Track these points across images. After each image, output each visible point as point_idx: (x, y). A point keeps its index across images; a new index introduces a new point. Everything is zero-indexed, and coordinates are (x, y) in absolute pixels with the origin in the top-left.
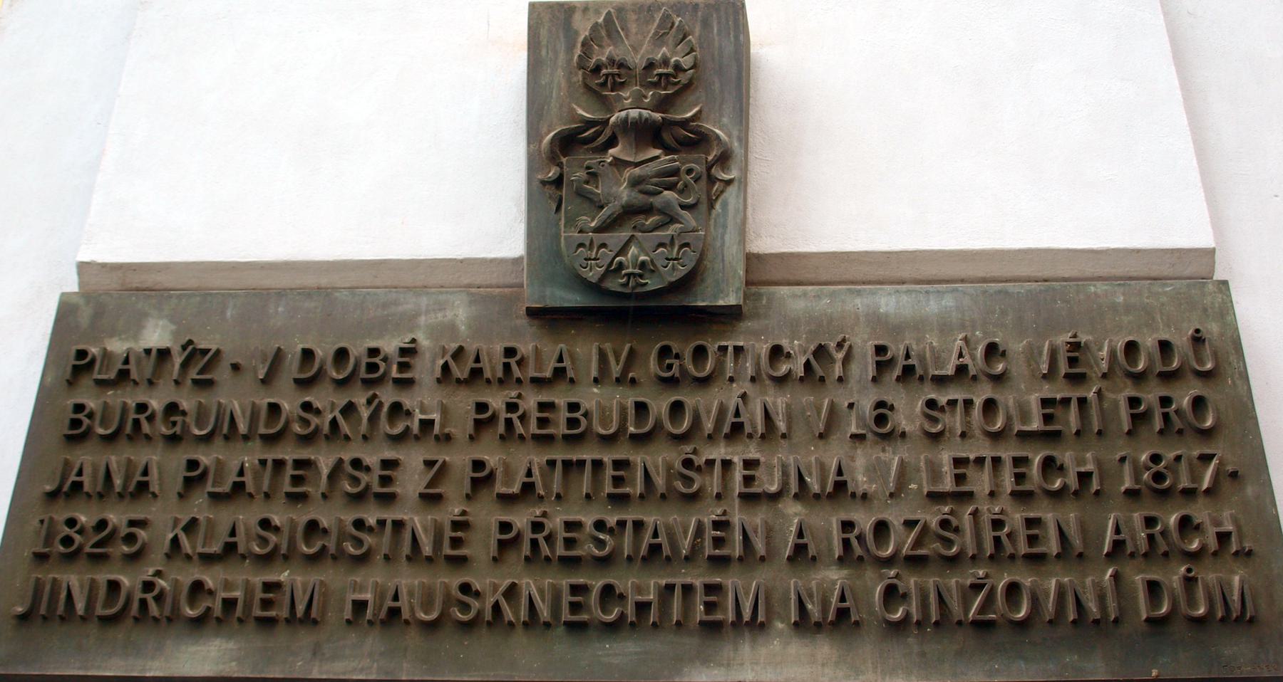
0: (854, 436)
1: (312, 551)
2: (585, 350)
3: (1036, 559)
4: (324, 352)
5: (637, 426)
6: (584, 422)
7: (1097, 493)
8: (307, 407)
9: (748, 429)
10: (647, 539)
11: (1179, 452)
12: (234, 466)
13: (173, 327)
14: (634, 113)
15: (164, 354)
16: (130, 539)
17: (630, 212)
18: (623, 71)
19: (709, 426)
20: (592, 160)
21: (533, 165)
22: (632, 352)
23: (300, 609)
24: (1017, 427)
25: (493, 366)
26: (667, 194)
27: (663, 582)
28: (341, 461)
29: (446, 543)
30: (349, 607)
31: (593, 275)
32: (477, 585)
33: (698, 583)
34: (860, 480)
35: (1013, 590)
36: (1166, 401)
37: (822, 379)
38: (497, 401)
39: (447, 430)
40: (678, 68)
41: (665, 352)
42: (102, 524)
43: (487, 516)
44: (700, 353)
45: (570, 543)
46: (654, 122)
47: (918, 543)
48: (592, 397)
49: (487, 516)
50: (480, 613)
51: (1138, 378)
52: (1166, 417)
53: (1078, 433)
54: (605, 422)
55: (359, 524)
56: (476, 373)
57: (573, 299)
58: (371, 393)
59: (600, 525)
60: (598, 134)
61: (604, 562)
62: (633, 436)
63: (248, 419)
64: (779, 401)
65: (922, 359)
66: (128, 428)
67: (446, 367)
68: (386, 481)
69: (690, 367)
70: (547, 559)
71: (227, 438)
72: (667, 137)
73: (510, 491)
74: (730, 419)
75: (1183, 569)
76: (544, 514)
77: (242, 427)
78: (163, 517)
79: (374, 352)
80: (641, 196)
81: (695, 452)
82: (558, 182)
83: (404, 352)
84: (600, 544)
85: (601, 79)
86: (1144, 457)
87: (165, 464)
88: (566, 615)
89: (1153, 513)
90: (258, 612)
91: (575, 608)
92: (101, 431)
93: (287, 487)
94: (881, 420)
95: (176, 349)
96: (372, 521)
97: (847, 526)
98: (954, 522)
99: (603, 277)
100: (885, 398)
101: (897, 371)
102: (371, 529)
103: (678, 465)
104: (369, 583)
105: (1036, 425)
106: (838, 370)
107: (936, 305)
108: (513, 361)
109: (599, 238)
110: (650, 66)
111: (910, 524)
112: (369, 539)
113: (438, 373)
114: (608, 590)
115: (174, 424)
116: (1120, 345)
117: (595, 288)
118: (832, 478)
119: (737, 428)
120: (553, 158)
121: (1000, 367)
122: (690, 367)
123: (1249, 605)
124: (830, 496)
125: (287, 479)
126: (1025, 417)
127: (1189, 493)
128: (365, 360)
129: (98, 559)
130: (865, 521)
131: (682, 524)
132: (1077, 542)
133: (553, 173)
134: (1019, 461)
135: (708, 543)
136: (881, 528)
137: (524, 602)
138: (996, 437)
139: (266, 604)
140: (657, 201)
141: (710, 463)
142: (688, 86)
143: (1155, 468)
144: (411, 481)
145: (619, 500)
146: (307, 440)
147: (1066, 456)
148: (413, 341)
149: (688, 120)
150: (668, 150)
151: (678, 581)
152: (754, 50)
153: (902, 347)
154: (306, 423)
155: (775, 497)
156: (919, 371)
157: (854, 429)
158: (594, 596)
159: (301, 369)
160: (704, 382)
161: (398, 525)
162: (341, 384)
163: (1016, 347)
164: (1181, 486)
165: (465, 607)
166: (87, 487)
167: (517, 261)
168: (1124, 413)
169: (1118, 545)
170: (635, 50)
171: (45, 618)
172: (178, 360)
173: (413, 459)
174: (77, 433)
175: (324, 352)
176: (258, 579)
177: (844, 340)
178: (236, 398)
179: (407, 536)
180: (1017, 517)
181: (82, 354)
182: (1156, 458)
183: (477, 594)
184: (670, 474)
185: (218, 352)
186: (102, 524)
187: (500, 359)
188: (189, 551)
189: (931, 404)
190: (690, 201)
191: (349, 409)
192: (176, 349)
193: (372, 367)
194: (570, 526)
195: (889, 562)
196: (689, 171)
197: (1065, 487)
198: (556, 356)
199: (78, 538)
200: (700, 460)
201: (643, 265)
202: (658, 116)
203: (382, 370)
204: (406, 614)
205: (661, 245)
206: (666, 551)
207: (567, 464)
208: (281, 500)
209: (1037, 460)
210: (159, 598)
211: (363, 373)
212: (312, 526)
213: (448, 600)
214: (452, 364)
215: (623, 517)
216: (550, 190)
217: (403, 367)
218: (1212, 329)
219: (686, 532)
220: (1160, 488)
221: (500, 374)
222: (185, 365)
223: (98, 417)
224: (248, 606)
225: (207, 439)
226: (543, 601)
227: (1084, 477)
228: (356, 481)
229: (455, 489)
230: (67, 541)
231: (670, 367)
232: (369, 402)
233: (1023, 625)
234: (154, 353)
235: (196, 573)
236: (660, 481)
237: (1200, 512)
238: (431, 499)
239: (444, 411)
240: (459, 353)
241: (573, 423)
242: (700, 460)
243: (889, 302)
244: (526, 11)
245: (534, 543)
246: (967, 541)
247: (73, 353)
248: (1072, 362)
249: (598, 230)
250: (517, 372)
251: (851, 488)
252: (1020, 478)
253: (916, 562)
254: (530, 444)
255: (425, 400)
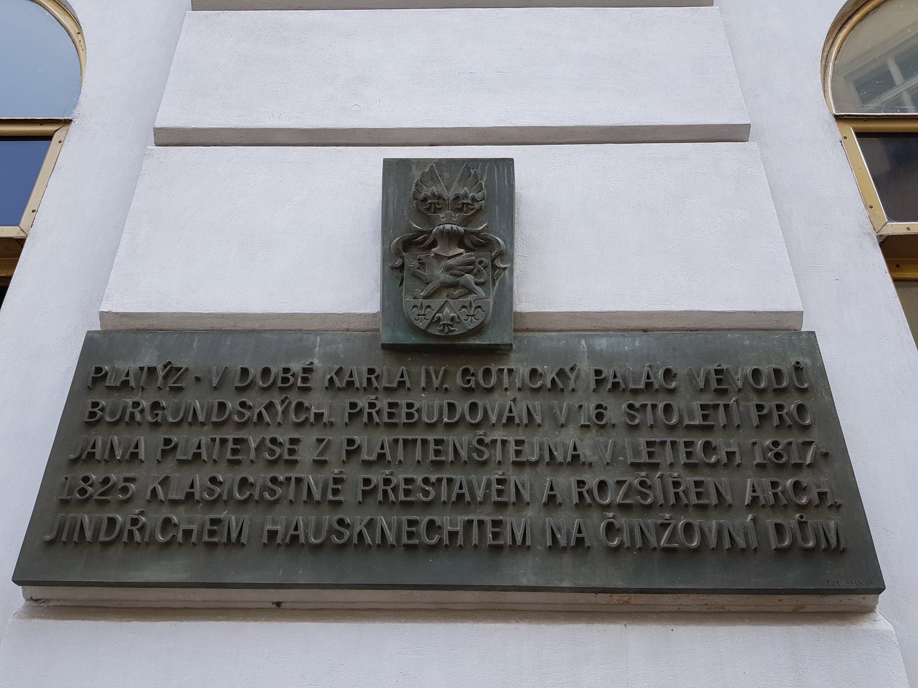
0: (582, 426)
1: (242, 498)
2: (420, 370)
3: (702, 508)
4: (255, 371)
5: (449, 419)
6: (416, 416)
7: (739, 465)
8: (243, 404)
9: (517, 421)
10: (456, 490)
11: (790, 440)
12: (195, 441)
13: (157, 353)
14: (448, 227)
15: (152, 371)
16: (125, 490)
17: (445, 286)
18: (441, 201)
19: (493, 419)
20: (422, 255)
21: (386, 257)
22: (446, 371)
23: (234, 536)
24: (687, 422)
25: (360, 381)
26: (469, 277)
27: (466, 518)
28: (264, 439)
29: (330, 492)
30: (265, 534)
31: (422, 325)
32: (348, 521)
33: (488, 519)
34: (586, 453)
35: (688, 527)
36: (780, 407)
37: (562, 390)
38: (362, 402)
39: (331, 420)
40: (473, 199)
41: (466, 372)
42: (106, 480)
43: (355, 474)
44: (487, 372)
45: (407, 492)
46: (459, 232)
47: (626, 496)
48: (422, 401)
49: (355, 474)
50: (350, 538)
51: (760, 392)
52: (780, 416)
53: (724, 426)
54: (430, 415)
55: (274, 480)
56: (350, 384)
57: (413, 340)
58: (284, 396)
59: (426, 481)
60: (425, 239)
61: (428, 505)
62: (446, 424)
63: (205, 412)
64: (537, 404)
65: (624, 379)
66: (127, 418)
67: (331, 380)
68: (292, 452)
69: (482, 381)
70: (393, 502)
71: (190, 424)
72: (467, 242)
73: (370, 458)
74: (506, 414)
75: (797, 515)
76: (392, 474)
77: (201, 418)
78: (147, 477)
79: (286, 370)
80: (451, 277)
81: (485, 434)
82: (401, 268)
83: (305, 370)
84: (426, 493)
85: (428, 207)
86: (768, 442)
87: (148, 442)
88: (405, 540)
89: (775, 479)
90: (206, 538)
91: (410, 535)
92: (108, 419)
93: (229, 456)
94: (600, 416)
95: (159, 367)
96: (281, 478)
97: (581, 483)
98: (649, 483)
99: (428, 327)
100: (602, 403)
101: (609, 386)
102: (281, 483)
103: (475, 443)
104: (278, 521)
105: (698, 421)
106: (572, 384)
107: (627, 345)
108: (373, 377)
109: (426, 302)
110: (457, 198)
111: (620, 483)
112: (279, 491)
113: (327, 384)
114: (431, 523)
115: (157, 415)
116: (749, 371)
117: (424, 333)
118: (570, 452)
119: (510, 419)
120: (398, 254)
121: (673, 385)
122: (482, 381)
123: (842, 541)
124: (569, 464)
125: (229, 452)
126: (691, 415)
127: (798, 467)
128: (281, 375)
129: (103, 503)
130: (592, 481)
131: (480, 481)
132: (728, 498)
133: (398, 262)
134: (688, 444)
135: (494, 493)
136: (602, 485)
137: (378, 531)
138: (672, 428)
139: (212, 533)
140: (461, 280)
141: (494, 442)
142: (479, 210)
143: (776, 450)
144: (307, 453)
145: (438, 465)
146: (242, 425)
147: (716, 440)
148: (312, 363)
149: (479, 232)
150: (468, 249)
151: (475, 518)
152: (518, 189)
153: (611, 371)
154: (241, 415)
155: (534, 464)
156: (623, 386)
157: (582, 423)
158: (423, 526)
159: (241, 380)
160: (490, 390)
161: (299, 481)
162: (264, 390)
163: (681, 370)
164: (793, 462)
165: (340, 535)
166: (98, 456)
167: (374, 315)
168: (754, 414)
169: (755, 499)
170: (448, 188)
171: (65, 543)
172: (161, 374)
173: (309, 437)
174: (93, 421)
175: (255, 371)
176: (208, 517)
177: (606, 409)
178: (197, 400)
179: (305, 488)
180: (688, 480)
181: (98, 370)
182: (775, 444)
183: (348, 526)
184: (471, 450)
185: (187, 369)
186: (106, 480)
187: (365, 376)
188: (163, 499)
189: (631, 406)
190: (481, 280)
191: (270, 406)
192: (159, 367)
193: (286, 380)
194: (408, 481)
195: (608, 507)
196: (481, 262)
197: (718, 461)
198: (399, 374)
199: (90, 489)
200: (487, 440)
201: (453, 319)
202: (461, 229)
203: (291, 382)
204: (302, 539)
205: (464, 307)
206: (468, 498)
207: (406, 442)
208: (223, 465)
209: (700, 443)
210: (142, 529)
211: (279, 384)
212: (244, 482)
213: (331, 531)
214: (335, 378)
215: (440, 476)
216: (397, 273)
217: (305, 380)
218: (806, 361)
219: (479, 486)
220: (778, 463)
221: (365, 385)
222: (165, 377)
223: (107, 410)
224: (200, 535)
225: (178, 424)
226: (390, 530)
227: (730, 455)
228: (272, 452)
229: (336, 455)
230: (83, 491)
231: (469, 381)
232: (283, 402)
233: (696, 550)
234: (146, 369)
235: (166, 512)
236: (464, 454)
237: (805, 478)
238: (320, 464)
239: (331, 407)
240: (339, 372)
241: (409, 416)
242: (487, 440)
243: (602, 343)
244: (382, 163)
245: (385, 492)
246: (655, 495)
247: (93, 369)
248: (719, 381)
249: (426, 297)
250: (375, 384)
251: (582, 459)
252: (689, 455)
253: (624, 508)
254: (382, 428)
255: (318, 402)
